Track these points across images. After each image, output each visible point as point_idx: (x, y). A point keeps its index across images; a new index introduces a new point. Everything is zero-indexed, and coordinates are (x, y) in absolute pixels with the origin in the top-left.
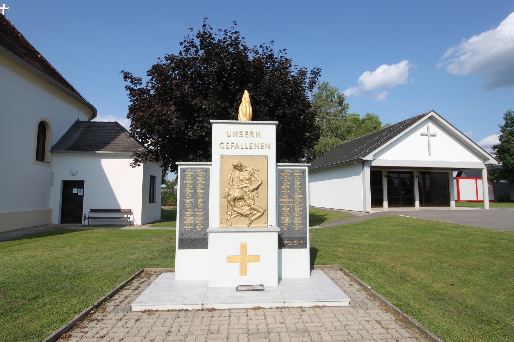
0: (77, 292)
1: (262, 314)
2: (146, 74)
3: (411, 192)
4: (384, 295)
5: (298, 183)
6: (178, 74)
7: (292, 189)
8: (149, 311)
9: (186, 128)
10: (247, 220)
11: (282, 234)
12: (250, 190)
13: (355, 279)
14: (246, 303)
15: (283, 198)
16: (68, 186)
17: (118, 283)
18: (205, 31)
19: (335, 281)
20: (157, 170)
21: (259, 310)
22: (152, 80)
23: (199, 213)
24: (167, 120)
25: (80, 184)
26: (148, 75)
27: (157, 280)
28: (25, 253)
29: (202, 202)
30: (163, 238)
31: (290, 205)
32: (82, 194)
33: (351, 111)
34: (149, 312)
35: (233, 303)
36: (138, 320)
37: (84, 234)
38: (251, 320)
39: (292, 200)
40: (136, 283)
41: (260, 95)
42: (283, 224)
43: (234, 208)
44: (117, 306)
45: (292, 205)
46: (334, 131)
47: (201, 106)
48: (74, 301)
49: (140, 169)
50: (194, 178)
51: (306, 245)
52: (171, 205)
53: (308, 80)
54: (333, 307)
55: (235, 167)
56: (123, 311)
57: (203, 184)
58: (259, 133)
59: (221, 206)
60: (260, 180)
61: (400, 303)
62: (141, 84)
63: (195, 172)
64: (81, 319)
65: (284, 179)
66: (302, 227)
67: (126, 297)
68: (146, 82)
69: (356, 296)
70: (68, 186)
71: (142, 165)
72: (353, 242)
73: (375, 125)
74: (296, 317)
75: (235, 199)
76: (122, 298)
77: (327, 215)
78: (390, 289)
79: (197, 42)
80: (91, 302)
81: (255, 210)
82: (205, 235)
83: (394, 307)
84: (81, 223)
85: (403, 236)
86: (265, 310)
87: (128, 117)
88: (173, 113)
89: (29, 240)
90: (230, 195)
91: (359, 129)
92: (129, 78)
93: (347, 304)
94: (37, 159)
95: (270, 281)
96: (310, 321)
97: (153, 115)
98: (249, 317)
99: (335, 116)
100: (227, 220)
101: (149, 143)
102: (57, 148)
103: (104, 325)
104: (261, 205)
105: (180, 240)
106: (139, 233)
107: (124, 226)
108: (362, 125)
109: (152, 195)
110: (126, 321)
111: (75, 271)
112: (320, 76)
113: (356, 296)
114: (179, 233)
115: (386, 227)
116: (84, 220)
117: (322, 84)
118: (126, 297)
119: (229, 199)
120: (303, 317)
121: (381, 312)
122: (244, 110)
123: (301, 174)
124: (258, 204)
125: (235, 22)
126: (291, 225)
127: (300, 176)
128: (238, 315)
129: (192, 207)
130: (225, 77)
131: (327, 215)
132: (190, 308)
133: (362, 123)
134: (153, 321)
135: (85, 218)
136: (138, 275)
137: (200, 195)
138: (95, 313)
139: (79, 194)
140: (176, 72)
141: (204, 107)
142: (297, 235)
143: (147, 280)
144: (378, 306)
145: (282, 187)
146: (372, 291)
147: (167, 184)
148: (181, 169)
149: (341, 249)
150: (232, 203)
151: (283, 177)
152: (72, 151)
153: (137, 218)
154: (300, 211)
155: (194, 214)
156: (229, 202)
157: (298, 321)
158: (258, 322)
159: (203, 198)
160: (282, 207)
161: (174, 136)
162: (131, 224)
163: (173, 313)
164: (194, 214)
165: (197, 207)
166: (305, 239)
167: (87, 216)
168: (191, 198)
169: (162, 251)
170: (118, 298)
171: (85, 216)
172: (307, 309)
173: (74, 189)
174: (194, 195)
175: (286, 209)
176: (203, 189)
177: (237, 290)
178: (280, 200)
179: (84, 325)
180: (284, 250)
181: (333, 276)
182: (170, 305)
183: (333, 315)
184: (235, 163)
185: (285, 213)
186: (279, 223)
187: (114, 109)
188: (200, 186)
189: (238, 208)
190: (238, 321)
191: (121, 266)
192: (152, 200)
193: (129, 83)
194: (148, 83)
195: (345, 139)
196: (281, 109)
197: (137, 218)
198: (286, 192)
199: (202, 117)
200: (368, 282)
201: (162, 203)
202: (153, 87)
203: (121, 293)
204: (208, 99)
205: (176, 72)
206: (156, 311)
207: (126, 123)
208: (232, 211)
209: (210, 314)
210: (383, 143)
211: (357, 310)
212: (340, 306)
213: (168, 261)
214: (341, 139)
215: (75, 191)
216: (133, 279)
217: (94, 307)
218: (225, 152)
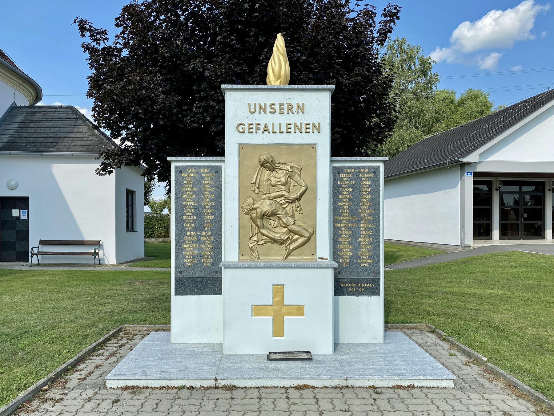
0: (22, 359)
1: (311, 396)
2: (115, 23)
3: (539, 215)
4: (512, 371)
5: (367, 190)
6: (164, 21)
7: (355, 201)
8: (133, 387)
9: (181, 110)
10: (282, 250)
11: (339, 273)
12: (287, 202)
13: (457, 346)
14: (284, 378)
15: (341, 215)
17: (84, 346)
19: (425, 348)
20: (137, 183)
21: (306, 391)
22: (123, 32)
24: (149, 97)
26: (117, 25)
27: (142, 342)
29: (212, 221)
30: (150, 282)
31: (352, 225)
32: (26, 218)
33: (441, 88)
34: (134, 390)
35: (264, 378)
36: (116, 401)
38: (294, 404)
39: (357, 218)
40: (111, 347)
41: (299, 51)
42: (341, 257)
43: (262, 231)
44: (84, 379)
45: (355, 225)
46: (415, 119)
47: (202, 73)
48: (18, 371)
49: (111, 179)
50: (198, 182)
51: (379, 290)
52: (160, 237)
53: (378, 27)
54: (427, 388)
55: (264, 164)
56: (93, 387)
58: (301, 106)
60: (303, 184)
61: (542, 384)
62: (107, 39)
63: (199, 173)
64: (29, 399)
65: (342, 183)
66: (372, 261)
67: (97, 367)
68: (113, 36)
69: (462, 372)
71: (113, 174)
72: (447, 290)
73: (479, 109)
74: (366, 401)
75: (264, 216)
76: (91, 368)
77: (401, 250)
78: (521, 363)
80: (44, 373)
81: (295, 233)
82: (216, 272)
83: (532, 391)
84: (28, 261)
85: (531, 282)
86: (316, 391)
87: (89, 95)
90: (256, 209)
91: (454, 116)
92: (87, 30)
93: (450, 384)
95: (323, 347)
96: (390, 410)
97: (126, 89)
98: (291, 401)
99: (414, 93)
100: (251, 248)
101: (124, 136)
103: (63, 408)
104: (305, 226)
105: (177, 280)
106: (112, 276)
108: (460, 109)
109: (130, 219)
110: (98, 402)
111: (18, 329)
112: (398, 18)
113: (462, 372)
114: (176, 270)
115: (500, 269)
116: (32, 257)
117: (395, 42)
118: (97, 367)
119: (254, 215)
120: (378, 402)
121: (509, 398)
122: (276, 68)
123: (371, 175)
126: (354, 258)
127: (370, 179)
128: (273, 396)
129: (194, 230)
130: (241, 22)
131: (401, 250)
132: (196, 384)
133: (459, 105)
134: (138, 403)
135: (33, 254)
136: (114, 336)
138: (50, 388)
139: (22, 218)
140: (162, 17)
141: (207, 74)
142: (364, 275)
143: (127, 343)
144: (503, 389)
145: (340, 197)
146: (490, 364)
147: (152, 207)
148: (176, 167)
149: (430, 301)
150: (259, 222)
151: (341, 180)
152: (8, 152)
153: (109, 255)
154: (370, 236)
155: (199, 239)
156: (253, 220)
157: (371, 408)
158: (305, 408)
159: (212, 214)
160: (340, 228)
163: (169, 391)
164: (199, 239)
165: (203, 229)
166: (377, 282)
167: (35, 251)
168: (194, 214)
169: (149, 301)
170: (85, 367)
171: (32, 251)
172: (384, 390)
173: (14, 211)
175: (345, 233)
177: (269, 358)
178: (337, 218)
179: (34, 408)
180: (343, 299)
181: (421, 341)
182: (165, 379)
183: (429, 401)
184: (263, 158)
185: (344, 239)
186: (335, 256)
187: (68, 88)
189: (269, 229)
190: (273, 406)
191: (88, 322)
192: (130, 228)
193: (87, 39)
194: (117, 37)
195: (430, 132)
197: (109, 255)
198: (345, 205)
199: (205, 91)
200: (481, 351)
201: (146, 233)
202: (126, 45)
203: (89, 361)
204: (214, 62)
205: (162, 17)
206: (144, 388)
207: (87, 110)
208: (260, 234)
209: (228, 394)
210: (497, 134)
211: (470, 394)
212: (438, 388)
213: (158, 314)
214: (424, 132)
215: (15, 213)
216: (107, 340)
217: (48, 381)
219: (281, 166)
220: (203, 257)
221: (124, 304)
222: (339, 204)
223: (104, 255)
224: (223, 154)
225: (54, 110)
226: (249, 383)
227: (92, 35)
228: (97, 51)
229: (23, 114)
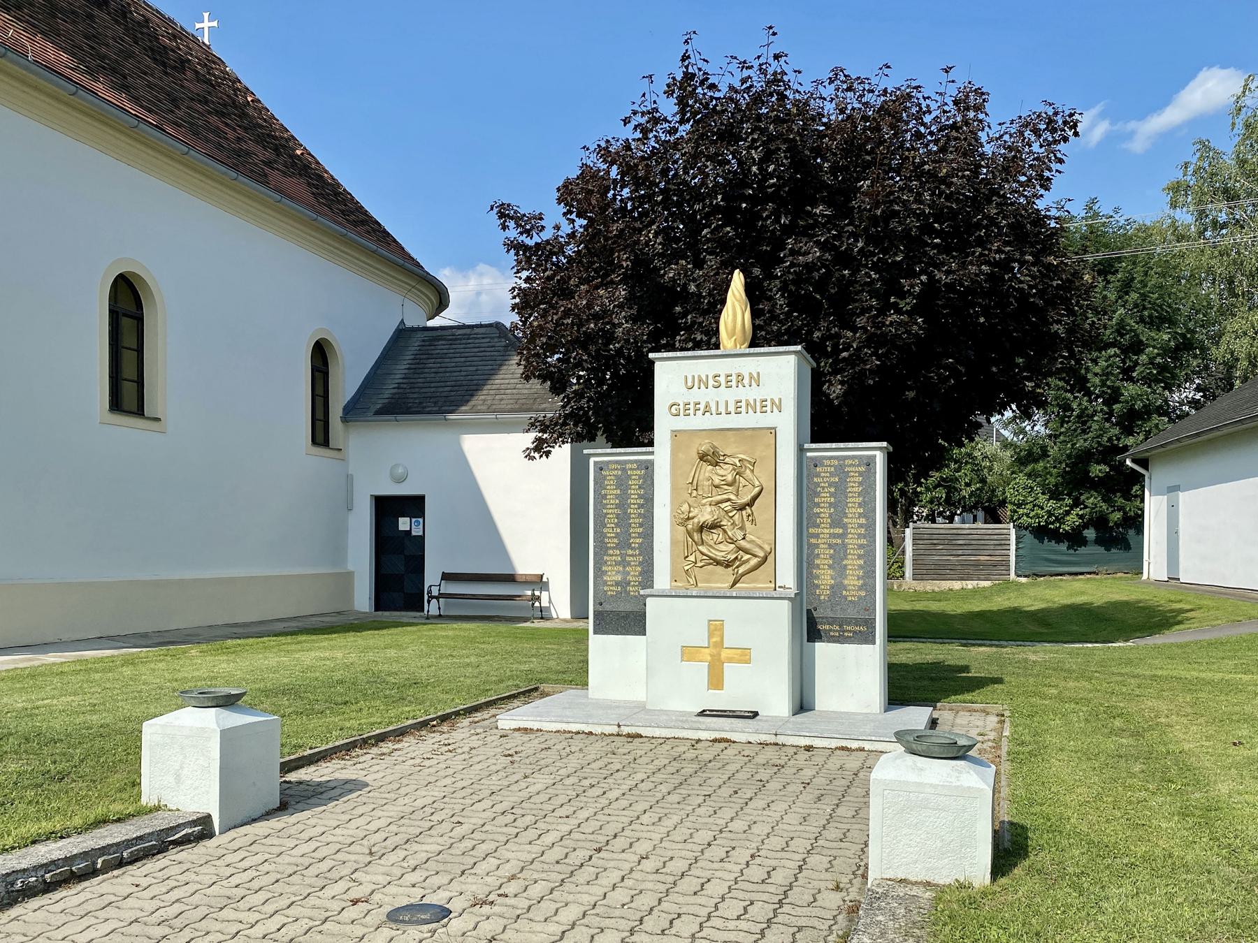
5: (856, 489)
7: (839, 507)
8: (526, 729)
10: (728, 575)
15: (818, 526)
16: (388, 509)
18: (690, 70)
23: (635, 559)
25: (415, 505)
28: (313, 654)
37: (427, 631)
45: (839, 541)
47: (685, 287)
55: (703, 457)
57: (640, 497)
59: (674, 543)
63: (624, 470)
66: (863, 594)
70: (388, 509)
75: (701, 528)
79: (669, 108)
88: (621, 306)
89: (314, 637)
92: (512, 218)
94: (314, 442)
95: (777, 703)
102: (353, 411)
105: (597, 615)
107: (526, 620)
116: (429, 602)
124: (755, 537)
125: (771, 28)
126: (837, 588)
127: (861, 474)
129: (618, 546)
132: (597, 730)
137: (634, 520)
139: (414, 533)
142: (852, 613)
148: (595, 463)
150: (696, 536)
151: (818, 475)
153: (558, 600)
154: (860, 557)
155: (624, 560)
156: (689, 534)
159: (641, 525)
160: (817, 546)
161: (623, 371)
162: (543, 615)
164: (624, 560)
166: (870, 623)
167: (435, 592)
168: (617, 525)
171: (430, 592)
173: (401, 528)
174: (623, 520)
176: (641, 506)
180: (822, 649)
185: (824, 559)
187: (483, 292)
188: (634, 499)
193: (513, 233)
196: (922, 272)
215: (404, 524)
218: (683, 423)
219: (727, 460)
220: (628, 583)
221: (552, 664)
222: (816, 510)
223: (550, 602)
224: (651, 443)
225: (468, 331)
226: (657, 732)
227: (518, 226)
228: (526, 248)
229: (415, 343)
